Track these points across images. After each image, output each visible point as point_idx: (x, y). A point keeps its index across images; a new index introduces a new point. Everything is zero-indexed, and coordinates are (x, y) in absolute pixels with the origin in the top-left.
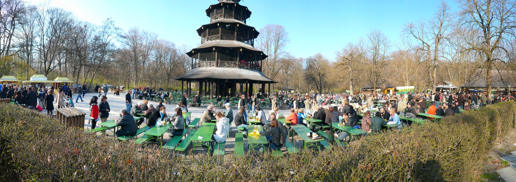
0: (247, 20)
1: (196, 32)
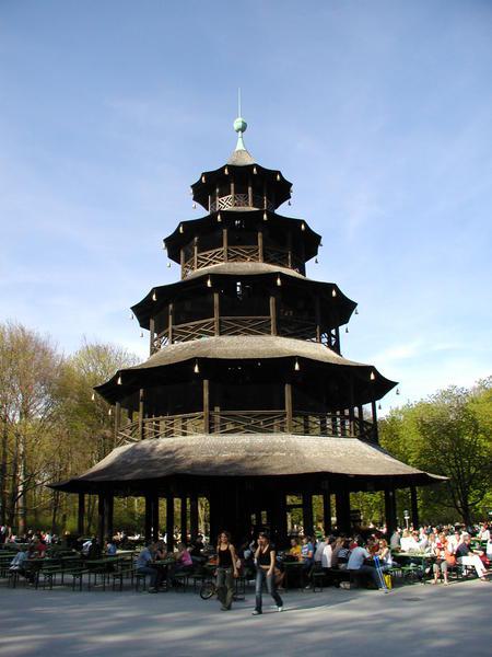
0: (309, 265)
1: (131, 313)
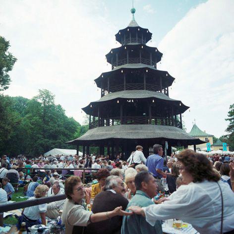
0: (158, 64)
